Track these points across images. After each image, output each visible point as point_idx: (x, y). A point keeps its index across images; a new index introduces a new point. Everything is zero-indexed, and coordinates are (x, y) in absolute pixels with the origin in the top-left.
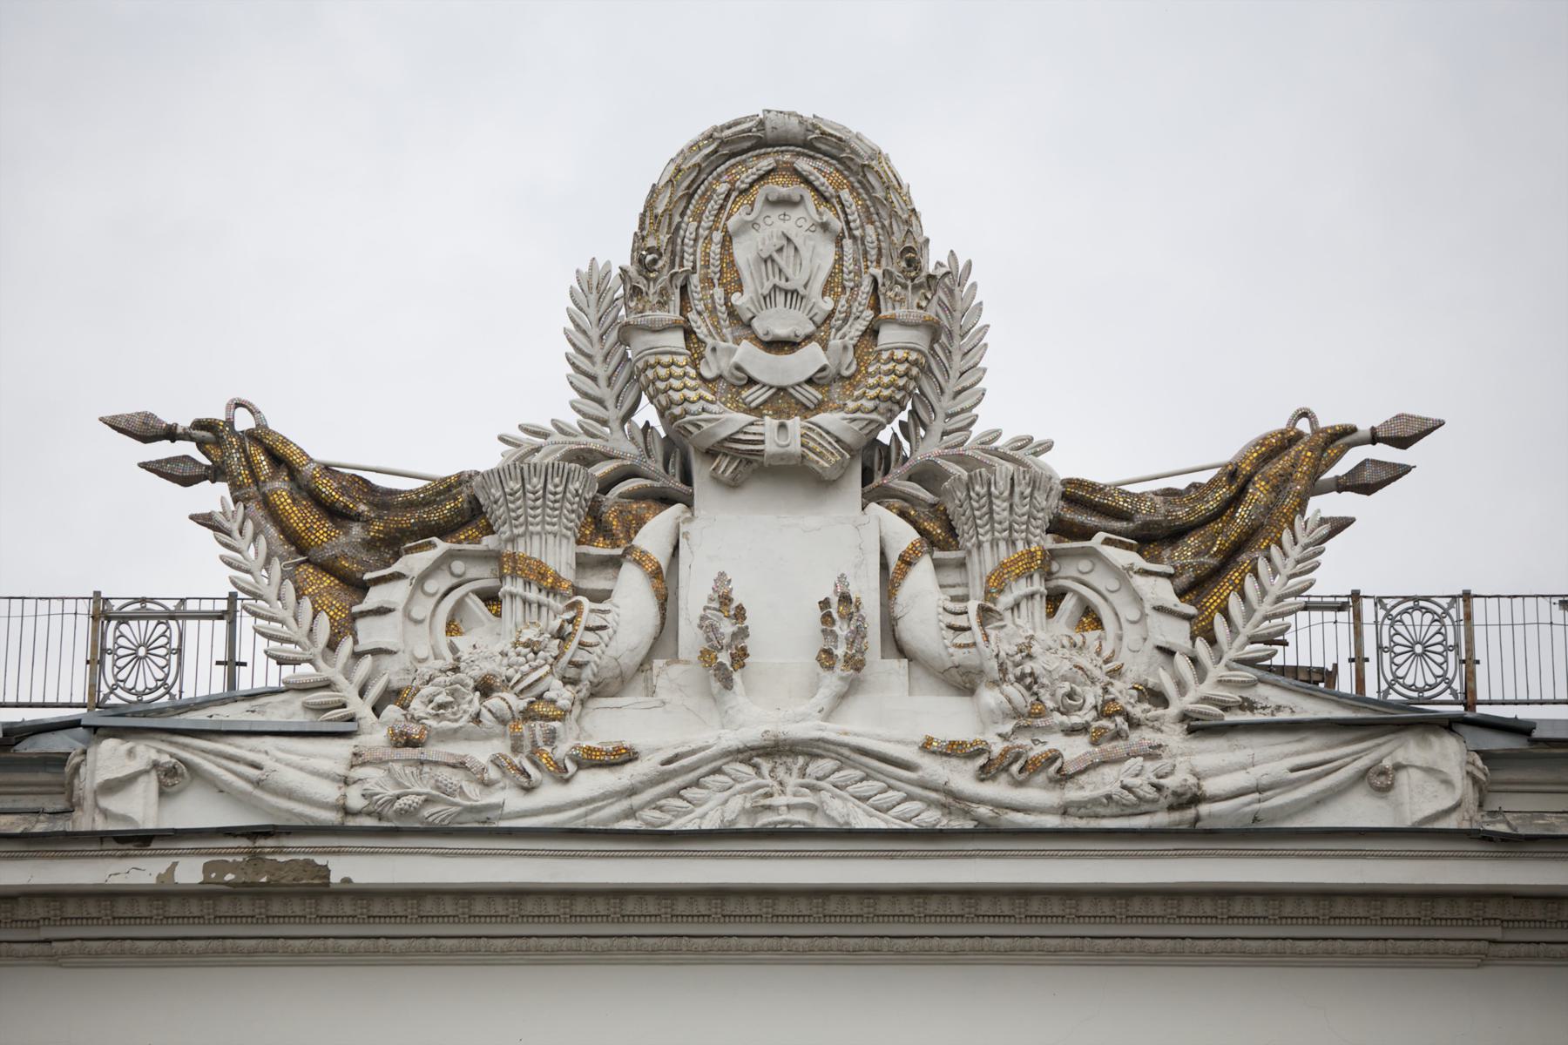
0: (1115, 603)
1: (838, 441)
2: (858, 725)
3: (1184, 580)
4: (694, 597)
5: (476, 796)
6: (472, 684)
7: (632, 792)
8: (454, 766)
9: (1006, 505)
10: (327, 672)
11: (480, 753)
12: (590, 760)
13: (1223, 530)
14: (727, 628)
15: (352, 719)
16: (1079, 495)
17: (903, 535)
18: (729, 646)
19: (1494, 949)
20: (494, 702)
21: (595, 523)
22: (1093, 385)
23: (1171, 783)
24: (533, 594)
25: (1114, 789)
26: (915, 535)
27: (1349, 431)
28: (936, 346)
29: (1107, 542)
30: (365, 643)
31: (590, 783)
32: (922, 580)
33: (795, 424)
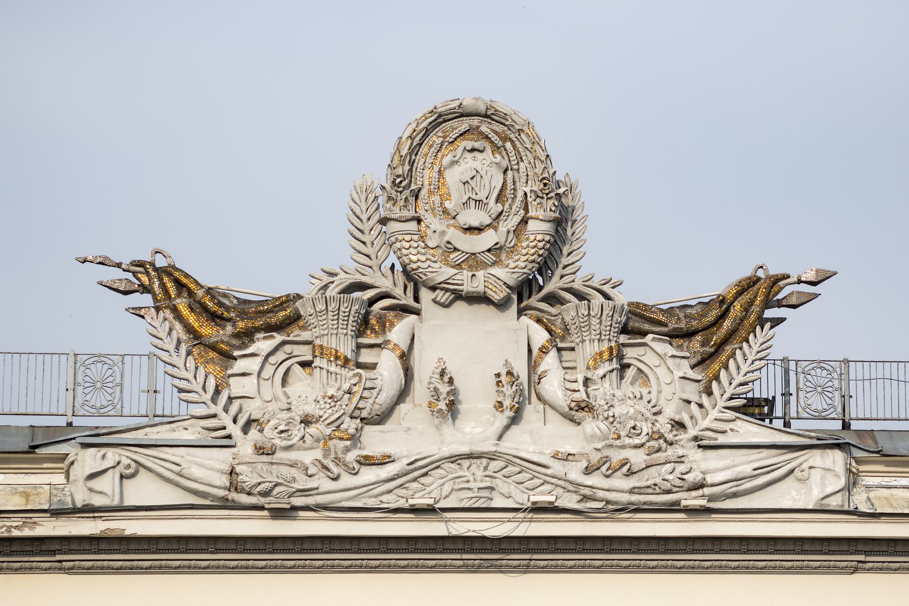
0: (658, 373)
1: (505, 283)
2: (520, 442)
3: (694, 361)
5: (303, 483)
6: (298, 419)
8: (291, 466)
9: (598, 321)
10: (213, 409)
11: (308, 457)
12: (367, 461)
13: (714, 330)
14: (444, 389)
15: (229, 437)
17: (540, 336)
18: (445, 399)
19: (860, 565)
20: (312, 430)
23: (690, 477)
24: (333, 368)
26: (546, 335)
28: (559, 228)
29: (654, 339)
30: (235, 392)
31: (369, 475)
33: (480, 274)
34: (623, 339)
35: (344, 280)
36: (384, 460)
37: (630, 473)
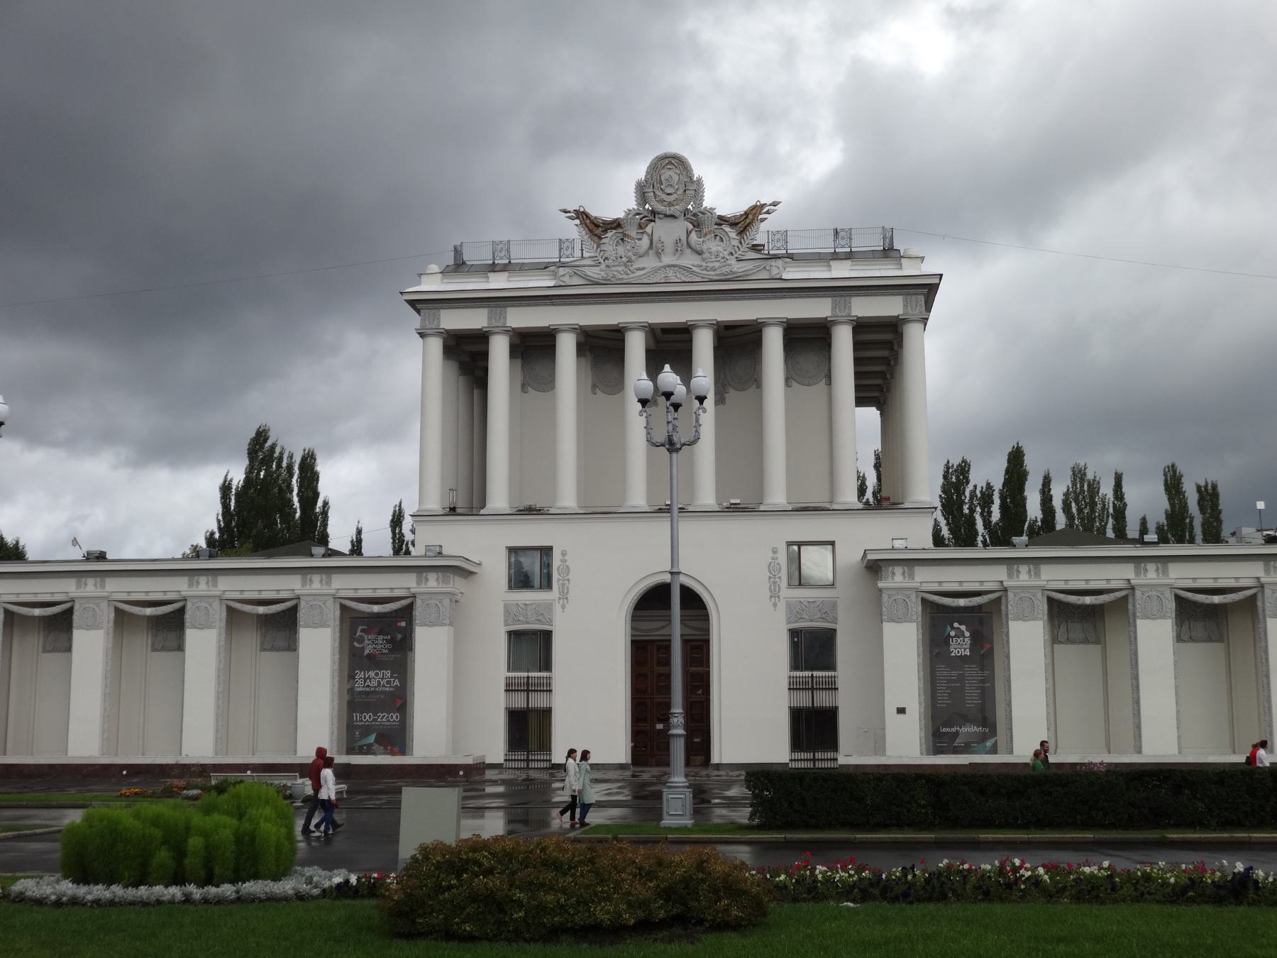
4: (655, 238)
12: (639, 269)
13: (745, 222)
16: (720, 217)
21: (640, 227)
22: (722, 194)
32: (694, 235)
36: (643, 269)
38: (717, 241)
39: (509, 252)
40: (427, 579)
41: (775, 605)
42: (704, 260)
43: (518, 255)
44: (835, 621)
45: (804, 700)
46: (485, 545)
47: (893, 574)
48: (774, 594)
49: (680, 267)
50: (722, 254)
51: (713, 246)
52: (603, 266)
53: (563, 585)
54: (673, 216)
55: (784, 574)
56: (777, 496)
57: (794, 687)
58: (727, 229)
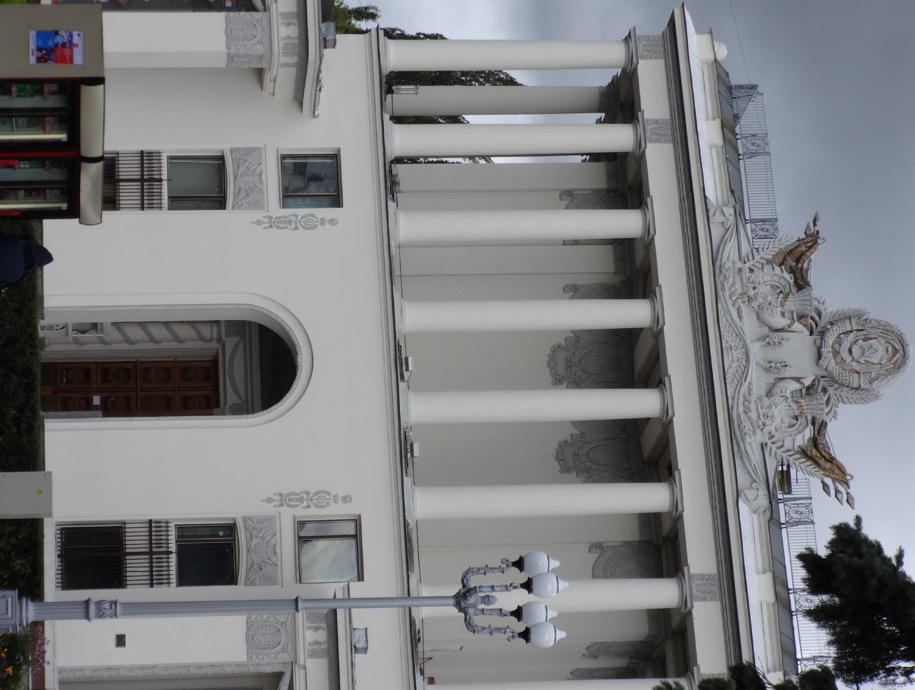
7: (732, 320)
12: (739, 312)
13: (818, 454)
16: (824, 425)
17: (807, 382)
20: (751, 290)
25: (744, 424)
27: (848, 487)
32: (795, 386)
33: (831, 355)
34: (810, 418)
35: (821, 308)
36: (740, 317)
37: (746, 412)
38: (788, 421)
39: (798, 523)
40: (289, 24)
41: (269, 500)
42: (760, 398)
43: (750, 168)
44: (249, 582)
45: (135, 541)
46: (341, 117)
47: (317, 629)
48: (285, 499)
49: (747, 367)
50: (771, 427)
51: (781, 412)
52: (739, 265)
53: (290, 222)
54: (820, 356)
55: (313, 512)
56: (427, 504)
57: (153, 527)
58: (808, 433)
